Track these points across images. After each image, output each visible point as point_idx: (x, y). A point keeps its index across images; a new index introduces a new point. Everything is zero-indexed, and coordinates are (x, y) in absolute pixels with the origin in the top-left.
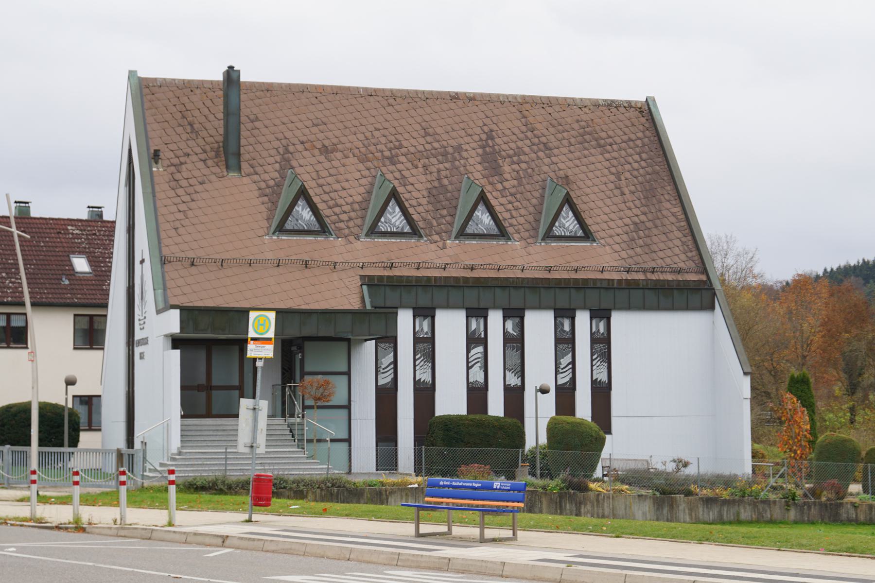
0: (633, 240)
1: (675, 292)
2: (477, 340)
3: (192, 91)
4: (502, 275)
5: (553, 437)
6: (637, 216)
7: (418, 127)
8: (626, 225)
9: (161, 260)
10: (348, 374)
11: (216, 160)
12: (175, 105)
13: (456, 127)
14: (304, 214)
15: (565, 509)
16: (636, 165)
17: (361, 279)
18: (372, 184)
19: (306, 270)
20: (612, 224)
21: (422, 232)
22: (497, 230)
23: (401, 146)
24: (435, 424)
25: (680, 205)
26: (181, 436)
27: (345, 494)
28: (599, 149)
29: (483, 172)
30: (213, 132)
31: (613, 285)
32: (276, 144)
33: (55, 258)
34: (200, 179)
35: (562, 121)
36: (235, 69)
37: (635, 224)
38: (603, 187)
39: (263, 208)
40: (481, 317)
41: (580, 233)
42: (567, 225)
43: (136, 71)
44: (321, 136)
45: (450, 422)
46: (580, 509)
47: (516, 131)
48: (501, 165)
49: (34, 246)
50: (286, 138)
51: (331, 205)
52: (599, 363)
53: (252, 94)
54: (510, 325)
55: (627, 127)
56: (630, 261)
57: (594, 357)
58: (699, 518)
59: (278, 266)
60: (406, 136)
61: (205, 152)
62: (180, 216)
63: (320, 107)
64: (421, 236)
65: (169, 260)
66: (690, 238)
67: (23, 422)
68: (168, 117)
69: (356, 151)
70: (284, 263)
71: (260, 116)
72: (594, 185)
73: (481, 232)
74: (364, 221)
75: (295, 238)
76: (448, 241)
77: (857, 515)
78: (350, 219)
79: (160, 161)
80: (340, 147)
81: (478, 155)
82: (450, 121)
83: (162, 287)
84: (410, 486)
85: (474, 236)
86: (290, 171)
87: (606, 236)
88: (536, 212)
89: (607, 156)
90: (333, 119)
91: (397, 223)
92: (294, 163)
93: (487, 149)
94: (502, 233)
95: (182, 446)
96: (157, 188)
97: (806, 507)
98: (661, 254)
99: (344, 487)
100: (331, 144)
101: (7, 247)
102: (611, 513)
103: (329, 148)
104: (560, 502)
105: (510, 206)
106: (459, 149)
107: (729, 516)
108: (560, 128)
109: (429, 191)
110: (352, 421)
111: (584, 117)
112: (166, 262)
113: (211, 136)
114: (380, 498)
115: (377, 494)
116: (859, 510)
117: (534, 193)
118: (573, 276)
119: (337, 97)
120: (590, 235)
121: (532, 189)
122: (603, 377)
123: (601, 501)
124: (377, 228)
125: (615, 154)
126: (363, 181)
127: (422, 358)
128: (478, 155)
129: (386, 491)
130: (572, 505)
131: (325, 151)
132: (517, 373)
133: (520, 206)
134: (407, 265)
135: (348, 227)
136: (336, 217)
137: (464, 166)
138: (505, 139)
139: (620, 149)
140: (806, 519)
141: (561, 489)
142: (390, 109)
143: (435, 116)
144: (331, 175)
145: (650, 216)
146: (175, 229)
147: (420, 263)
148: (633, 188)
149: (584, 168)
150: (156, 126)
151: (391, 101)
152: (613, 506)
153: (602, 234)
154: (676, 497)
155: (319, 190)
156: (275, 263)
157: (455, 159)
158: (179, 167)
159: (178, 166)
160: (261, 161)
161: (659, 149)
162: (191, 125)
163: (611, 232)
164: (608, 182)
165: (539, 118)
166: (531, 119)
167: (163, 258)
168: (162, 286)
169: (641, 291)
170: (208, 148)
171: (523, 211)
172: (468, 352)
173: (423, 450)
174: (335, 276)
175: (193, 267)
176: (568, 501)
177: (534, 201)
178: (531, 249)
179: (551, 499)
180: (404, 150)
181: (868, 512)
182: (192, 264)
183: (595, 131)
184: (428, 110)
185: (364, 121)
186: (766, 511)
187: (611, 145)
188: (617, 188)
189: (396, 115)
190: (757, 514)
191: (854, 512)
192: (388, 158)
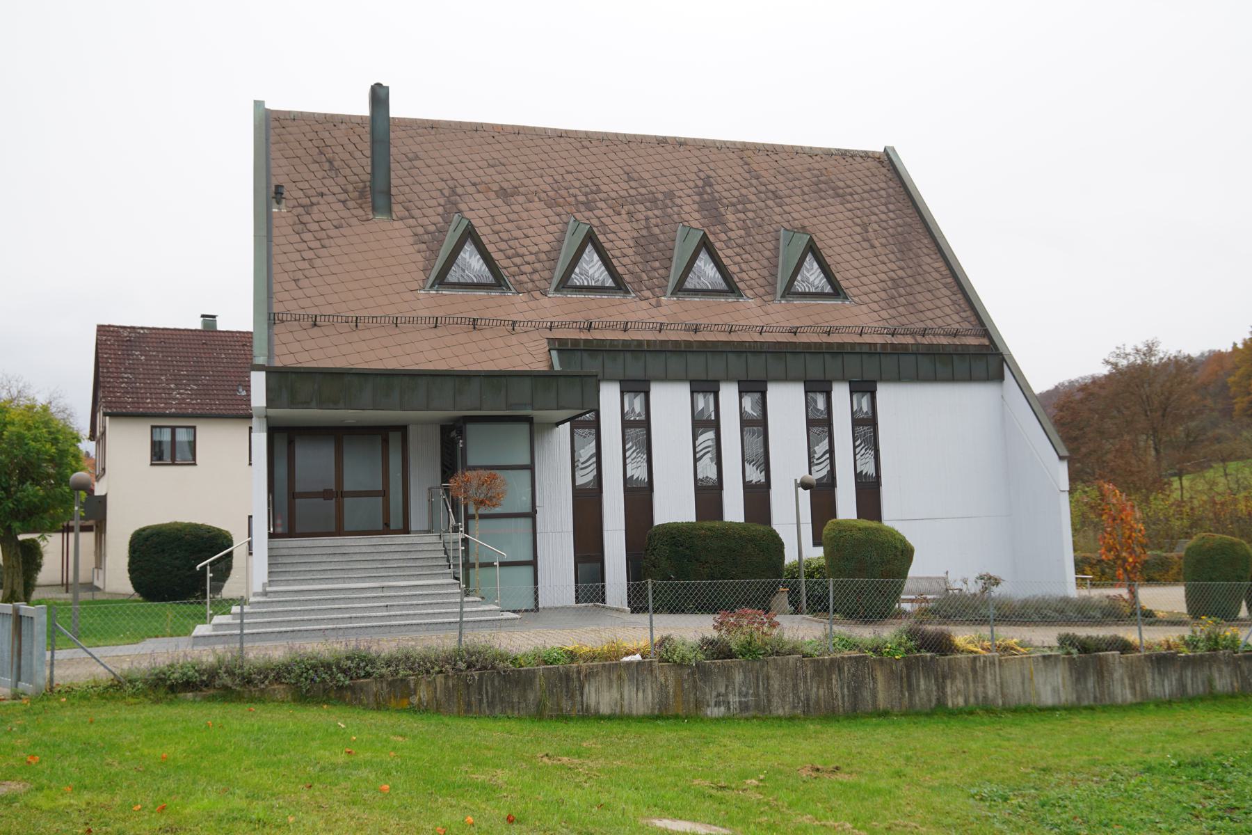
0: (893, 298)
2: (705, 423)
3: (335, 126)
4: (734, 338)
5: (837, 550)
6: (893, 271)
7: (619, 171)
8: (882, 281)
9: (269, 319)
10: (531, 468)
11: (359, 201)
12: (311, 140)
13: (666, 172)
14: (471, 264)
15: (918, 689)
16: (883, 217)
17: (549, 343)
18: (563, 232)
20: (864, 280)
21: (629, 287)
22: (724, 284)
23: (599, 191)
24: (657, 537)
25: (941, 259)
26: (269, 564)
27: (496, 683)
28: (838, 199)
29: (702, 221)
30: (358, 170)
31: (876, 349)
32: (441, 185)
33: (236, 370)
34: (335, 223)
35: (792, 170)
37: (893, 280)
38: (849, 239)
39: (419, 257)
40: (710, 392)
41: (609, 282)
42: (811, 279)
43: (263, 102)
44: (498, 178)
45: (675, 532)
46: (944, 688)
47: (738, 178)
49: (214, 358)
50: (453, 179)
51: (510, 255)
52: (863, 450)
53: (413, 131)
54: (748, 402)
55: (868, 177)
56: (892, 321)
57: (857, 443)
59: (436, 327)
60: (605, 180)
61: (346, 192)
62: (306, 265)
63: (498, 147)
64: (627, 292)
65: (280, 318)
66: (960, 296)
67: (155, 547)
68: (300, 152)
69: (543, 195)
70: (443, 322)
71: (421, 154)
72: (837, 237)
74: (553, 273)
75: (460, 293)
76: (663, 298)
78: (535, 271)
79: (284, 200)
80: (521, 190)
81: (694, 202)
82: (656, 165)
83: (266, 353)
84: (626, 659)
85: (696, 292)
86: (457, 215)
87: (860, 293)
88: (770, 265)
89: (849, 206)
90: (515, 161)
92: (462, 206)
93: (705, 196)
94: (732, 289)
95: (269, 581)
96: (275, 232)
98: (929, 314)
99: (493, 667)
100: (511, 187)
101: (182, 359)
103: (508, 190)
104: (909, 677)
105: (738, 259)
106: (670, 195)
107: (1195, 686)
108: (790, 176)
109: (636, 240)
110: (538, 535)
111: (817, 166)
112: (277, 322)
113: (355, 175)
114: (567, 686)
115: (561, 679)
117: (765, 244)
118: (825, 339)
119: (520, 137)
120: (840, 292)
121: (763, 240)
122: (869, 469)
123: (980, 671)
125: (857, 205)
126: (551, 228)
127: (634, 448)
128: (694, 202)
129: (579, 672)
130: (930, 681)
131: (503, 194)
133: (751, 259)
134: (611, 327)
135: (532, 281)
136: (516, 268)
137: (678, 214)
138: (726, 186)
139: (863, 199)
141: (908, 651)
142: (585, 152)
143: (640, 160)
144: (510, 221)
145: (909, 272)
146: (294, 280)
147: (627, 323)
148: (884, 241)
149: (823, 219)
150: (283, 162)
151: (586, 143)
152: (1001, 678)
153: (855, 291)
154: (1106, 658)
155: (494, 238)
156: (431, 322)
157: (667, 207)
158: (309, 208)
159: (307, 208)
160: (419, 204)
161: (907, 200)
162: (330, 162)
163: (865, 289)
164: (852, 233)
165: (764, 165)
166: (755, 166)
167: (272, 316)
168: (266, 352)
169: (913, 357)
170: (350, 188)
171: (754, 265)
172: (695, 439)
173: (650, 587)
174: (514, 340)
175: (316, 328)
177: (767, 253)
178: (769, 308)
179: (892, 671)
180: (602, 196)
183: (831, 179)
184: (631, 154)
185: (553, 164)
187: (851, 195)
188: (864, 240)
189: (593, 159)
190: (1239, 680)
192: (583, 203)
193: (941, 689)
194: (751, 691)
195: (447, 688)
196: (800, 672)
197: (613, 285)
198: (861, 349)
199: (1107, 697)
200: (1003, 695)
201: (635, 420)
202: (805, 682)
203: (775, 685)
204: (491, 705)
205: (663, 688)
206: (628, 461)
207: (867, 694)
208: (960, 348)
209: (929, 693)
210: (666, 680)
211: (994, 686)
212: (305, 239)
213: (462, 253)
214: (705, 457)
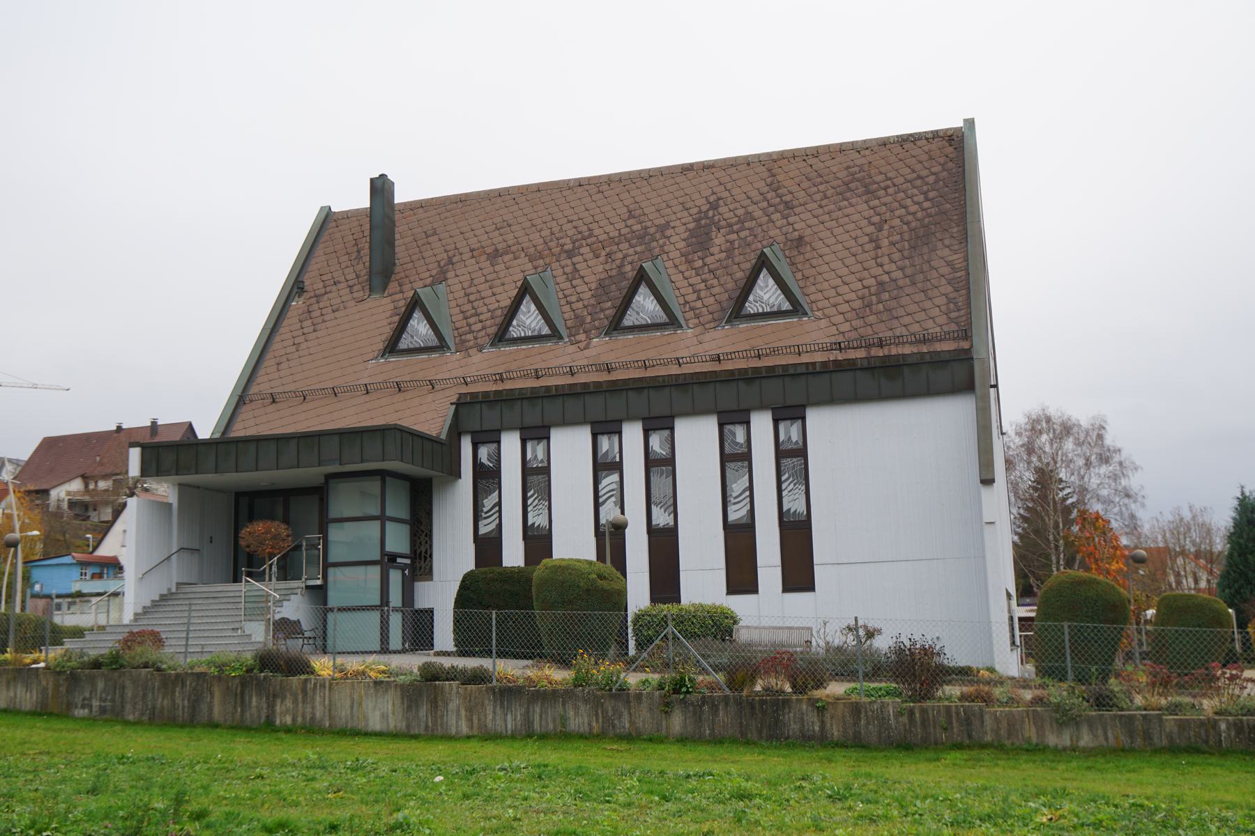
1: (906, 369)
2: (604, 466)
31: (815, 369)
37: (881, 284)
41: (786, 306)
43: (372, 180)
48: (713, 237)
52: (792, 486)
54: (656, 442)
58: (486, 726)
102: (327, 713)
104: (242, 693)
107: (543, 723)
124: (508, 334)
127: (536, 495)
130: (261, 699)
132: (667, 508)
134: (484, 378)
140: (708, 732)
152: (330, 701)
176: (254, 693)
179: (228, 688)
181: (849, 719)
182: (274, 401)
186: (620, 716)
190: (600, 721)
191: (816, 720)
193: (271, 707)
194: (109, 698)
196: (150, 683)
197: (791, 308)
198: (795, 370)
199: (439, 728)
200: (331, 718)
201: (537, 467)
202: (153, 693)
203: (129, 693)
205: (45, 690)
206: (784, 493)
207: (204, 708)
209: (259, 709)
210: (48, 684)
211: (322, 708)
212: (814, 265)
213: (411, 321)
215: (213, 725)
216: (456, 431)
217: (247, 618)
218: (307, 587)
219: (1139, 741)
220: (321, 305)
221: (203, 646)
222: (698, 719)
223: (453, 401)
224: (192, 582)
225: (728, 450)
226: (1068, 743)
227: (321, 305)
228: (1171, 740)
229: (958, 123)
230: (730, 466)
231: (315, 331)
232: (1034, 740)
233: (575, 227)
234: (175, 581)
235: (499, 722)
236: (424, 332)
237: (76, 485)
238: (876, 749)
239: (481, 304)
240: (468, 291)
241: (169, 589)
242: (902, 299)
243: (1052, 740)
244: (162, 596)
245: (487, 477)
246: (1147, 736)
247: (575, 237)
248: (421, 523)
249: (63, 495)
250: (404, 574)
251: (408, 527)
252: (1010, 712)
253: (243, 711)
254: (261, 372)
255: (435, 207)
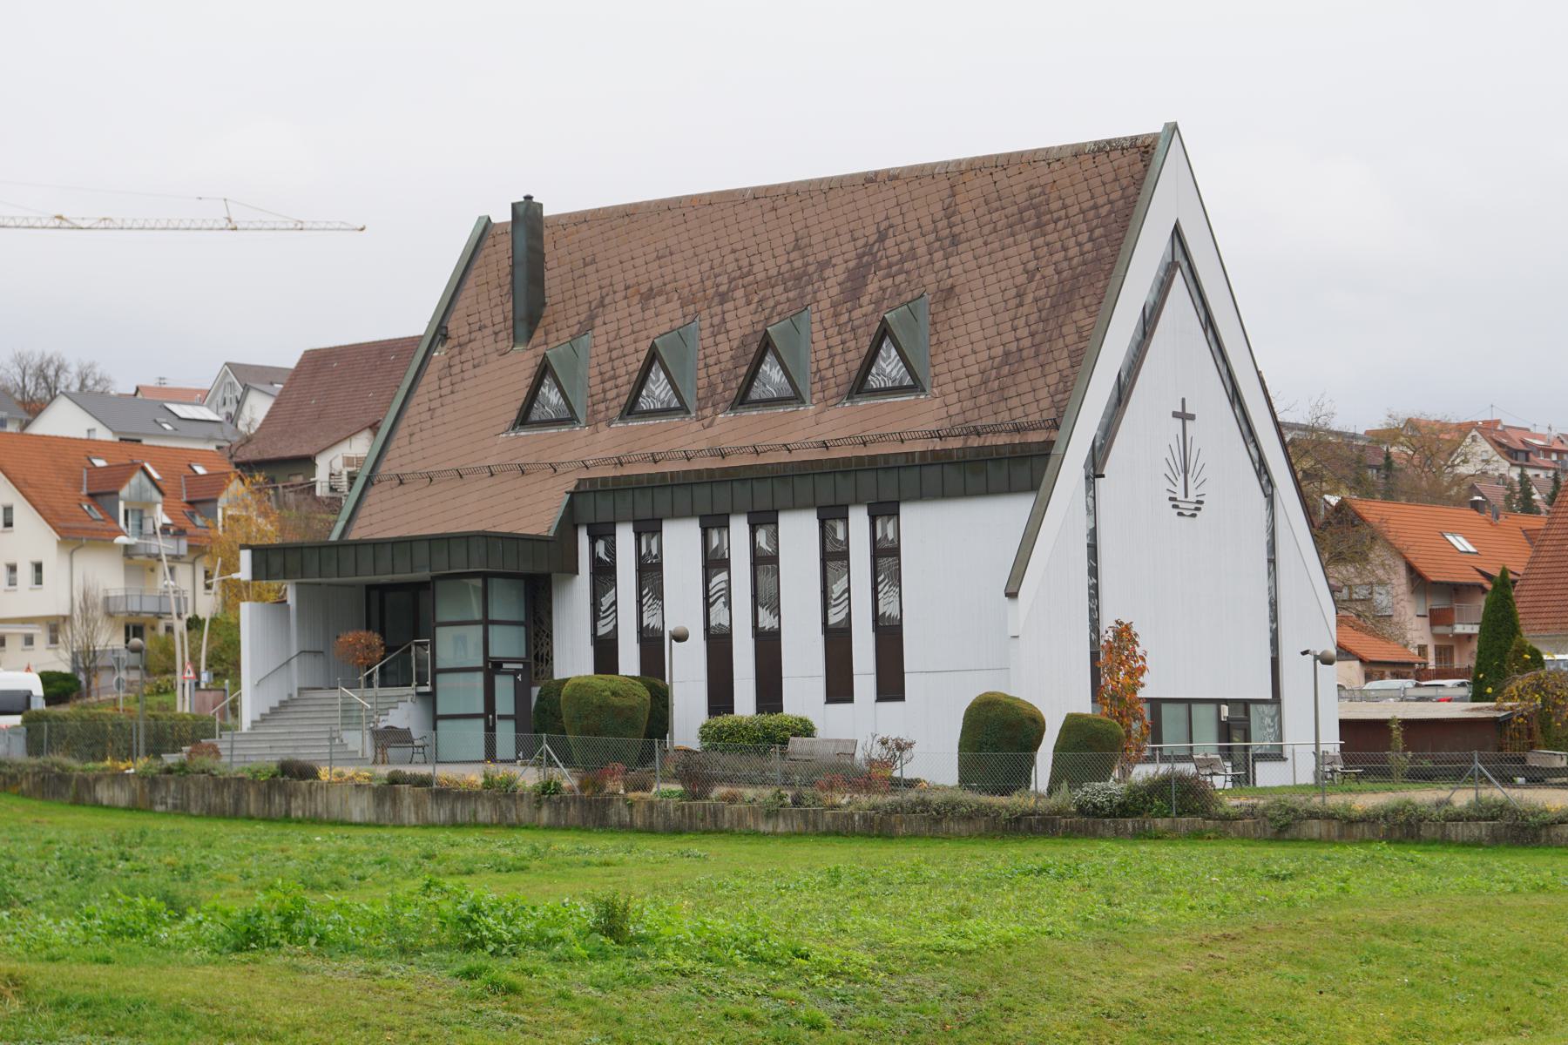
2: (715, 563)
19: (524, 477)
31: (914, 460)
36: (534, 200)
42: (888, 370)
43: (514, 205)
52: (887, 587)
73: (771, 396)
75: (651, 422)
77: (631, 819)
91: (662, 396)
97: (562, 805)
116: (635, 810)
123: (314, 793)
134: (740, 450)
169: (918, 469)
182: (401, 483)
186: (510, 810)
193: (288, 803)
195: (33, 783)
200: (328, 812)
203: (193, 793)
204: (53, 794)
205: (134, 791)
206: (880, 596)
207: (244, 804)
208: (1018, 449)
209: (280, 805)
214: (719, 601)
215: (250, 818)
216: (569, 524)
217: (344, 727)
218: (418, 694)
219: (811, 828)
220: (463, 358)
221: (245, 756)
222: (558, 813)
223: (568, 490)
224: (317, 686)
225: (829, 548)
226: (771, 830)
227: (463, 358)
228: (828, 827)
229: (1157, 127)
230: (831, 564)
231: (452, 392)
232: (752, 828)
233: (737, 260)
234: (296, 687)
235: (435, 815)
236: (555, 401)
237: (361, 447)
238: (662, 834)
239: (622, 364)
240: (613, 345)
241: (290, 695)
242: (1020, 375)
243: (762, 827)
244: (271, 709)
245: (604, 573)
246: (815, 826)
247: (733, 275)
248: (542, 623)
249: (338, 465)
250: (516, 680)
251: (523, 629)
252: (740, 809)
253: (269, 807)
254: (393, 445)
255: (601, 222)
